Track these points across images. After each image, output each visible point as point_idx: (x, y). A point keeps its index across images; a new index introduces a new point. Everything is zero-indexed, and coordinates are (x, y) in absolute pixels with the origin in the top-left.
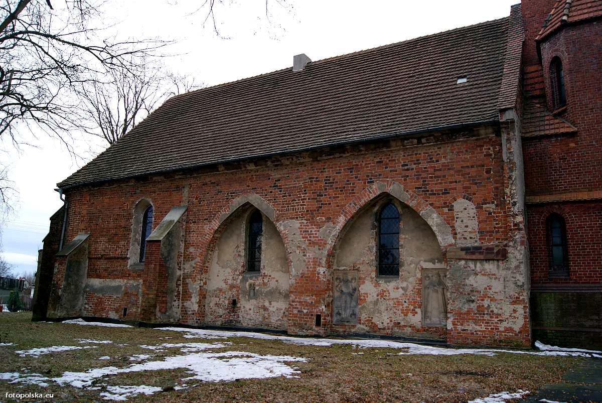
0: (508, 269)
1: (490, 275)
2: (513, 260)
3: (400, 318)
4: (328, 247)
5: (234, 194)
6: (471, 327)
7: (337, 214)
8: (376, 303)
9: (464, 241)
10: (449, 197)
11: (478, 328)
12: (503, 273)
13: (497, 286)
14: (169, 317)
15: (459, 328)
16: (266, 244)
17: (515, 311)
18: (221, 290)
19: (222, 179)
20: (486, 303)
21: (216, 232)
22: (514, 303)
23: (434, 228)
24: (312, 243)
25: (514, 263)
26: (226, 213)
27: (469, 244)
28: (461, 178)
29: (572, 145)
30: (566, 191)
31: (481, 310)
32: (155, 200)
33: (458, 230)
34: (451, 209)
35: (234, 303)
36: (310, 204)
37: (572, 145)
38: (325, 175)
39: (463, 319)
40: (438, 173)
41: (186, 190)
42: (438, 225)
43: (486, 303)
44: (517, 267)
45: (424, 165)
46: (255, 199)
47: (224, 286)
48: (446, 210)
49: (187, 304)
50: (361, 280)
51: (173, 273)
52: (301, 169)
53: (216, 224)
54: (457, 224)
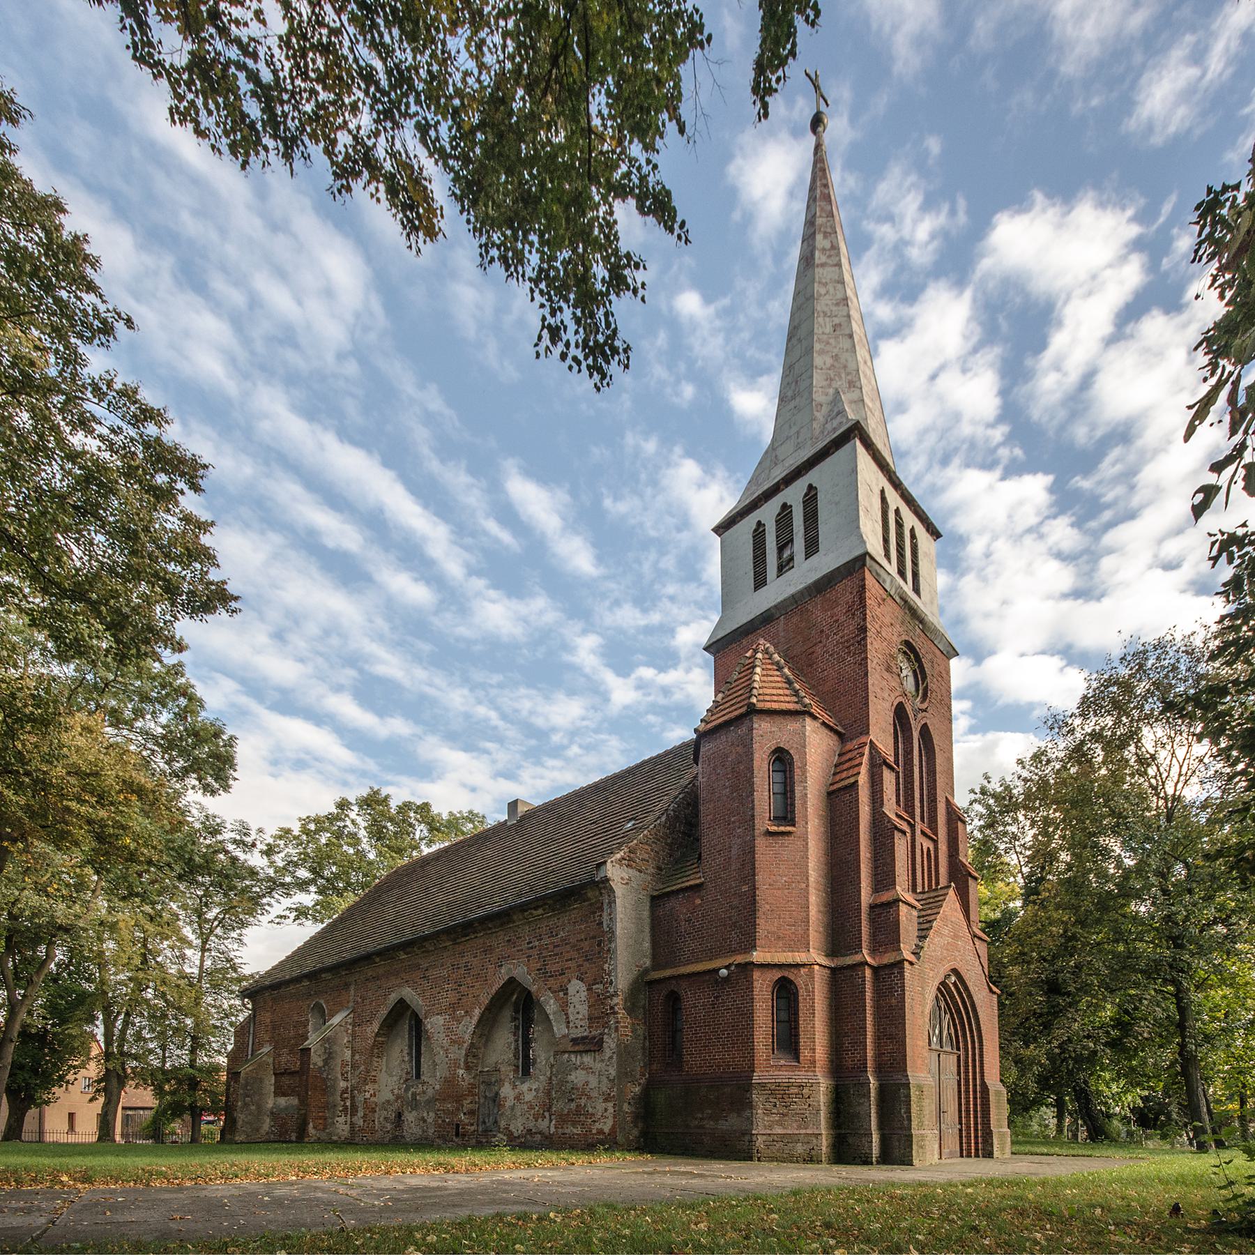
0: (602, 1061)
1: (588, 1069)
2: (607, 1050)
3: (531, 1125)
4: (466, 1045)
5: (390, 990)
6: (571, 1130)
7: (473, 1009)
8: (513, 1108)
9: (575, 1031)
10: (564, 979)
11: (575, 1131)
12: (598, 1066)
13: (593, 1081)
14: (330, 1134)
15: (560, 1131)
16: (536, 1030)
17: (606, 1110)
18: (388, 1101)
19: (381, 971)
20: (583, 1102)
21: (377, 1035)
22: (606, 1100)
23: (551, 1017)
24: (453, 1042)
25: (608, 1053)
26: (384, 1012)
27: (579, 1033)
28: (575, 955)
29: (698, 901)
30: (689, 962)
31: (579, 1111)
32: (327, 1002)
33: (571, 1018)
34: (565, 991)
35: (399, 1115)
36: (452, 997)
37: (698, 901)
38: (465, 959)
39: (564, 1121)
40: (557, 950)
41: (352, 987)
42: (554, 1013)
43: (583, 1102)
44: (611, 1058)
45: (546, 941)
46: (408, 993)
47: (392, 1098)
48: (561, 994)
49: (355, 1119)
50: (500, 1082)
51: (334, 1087)
52: (445, 955)
53: (375, 1027)
54: (571, 1010)
